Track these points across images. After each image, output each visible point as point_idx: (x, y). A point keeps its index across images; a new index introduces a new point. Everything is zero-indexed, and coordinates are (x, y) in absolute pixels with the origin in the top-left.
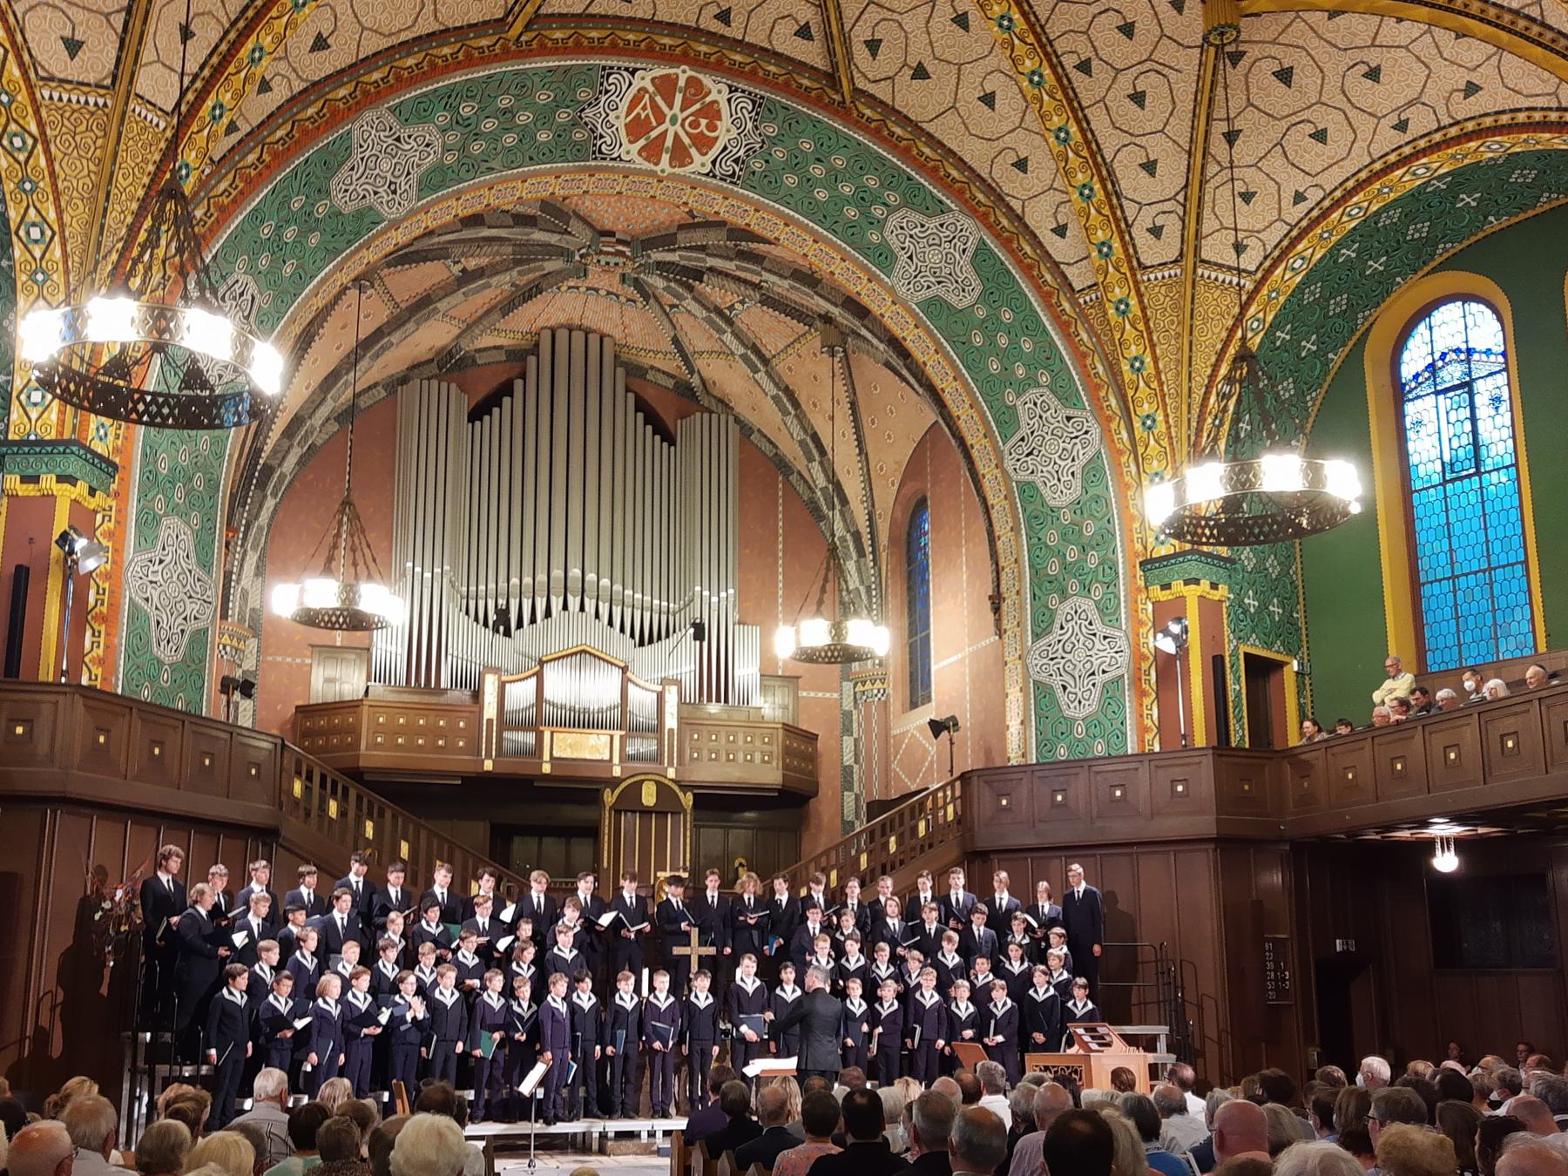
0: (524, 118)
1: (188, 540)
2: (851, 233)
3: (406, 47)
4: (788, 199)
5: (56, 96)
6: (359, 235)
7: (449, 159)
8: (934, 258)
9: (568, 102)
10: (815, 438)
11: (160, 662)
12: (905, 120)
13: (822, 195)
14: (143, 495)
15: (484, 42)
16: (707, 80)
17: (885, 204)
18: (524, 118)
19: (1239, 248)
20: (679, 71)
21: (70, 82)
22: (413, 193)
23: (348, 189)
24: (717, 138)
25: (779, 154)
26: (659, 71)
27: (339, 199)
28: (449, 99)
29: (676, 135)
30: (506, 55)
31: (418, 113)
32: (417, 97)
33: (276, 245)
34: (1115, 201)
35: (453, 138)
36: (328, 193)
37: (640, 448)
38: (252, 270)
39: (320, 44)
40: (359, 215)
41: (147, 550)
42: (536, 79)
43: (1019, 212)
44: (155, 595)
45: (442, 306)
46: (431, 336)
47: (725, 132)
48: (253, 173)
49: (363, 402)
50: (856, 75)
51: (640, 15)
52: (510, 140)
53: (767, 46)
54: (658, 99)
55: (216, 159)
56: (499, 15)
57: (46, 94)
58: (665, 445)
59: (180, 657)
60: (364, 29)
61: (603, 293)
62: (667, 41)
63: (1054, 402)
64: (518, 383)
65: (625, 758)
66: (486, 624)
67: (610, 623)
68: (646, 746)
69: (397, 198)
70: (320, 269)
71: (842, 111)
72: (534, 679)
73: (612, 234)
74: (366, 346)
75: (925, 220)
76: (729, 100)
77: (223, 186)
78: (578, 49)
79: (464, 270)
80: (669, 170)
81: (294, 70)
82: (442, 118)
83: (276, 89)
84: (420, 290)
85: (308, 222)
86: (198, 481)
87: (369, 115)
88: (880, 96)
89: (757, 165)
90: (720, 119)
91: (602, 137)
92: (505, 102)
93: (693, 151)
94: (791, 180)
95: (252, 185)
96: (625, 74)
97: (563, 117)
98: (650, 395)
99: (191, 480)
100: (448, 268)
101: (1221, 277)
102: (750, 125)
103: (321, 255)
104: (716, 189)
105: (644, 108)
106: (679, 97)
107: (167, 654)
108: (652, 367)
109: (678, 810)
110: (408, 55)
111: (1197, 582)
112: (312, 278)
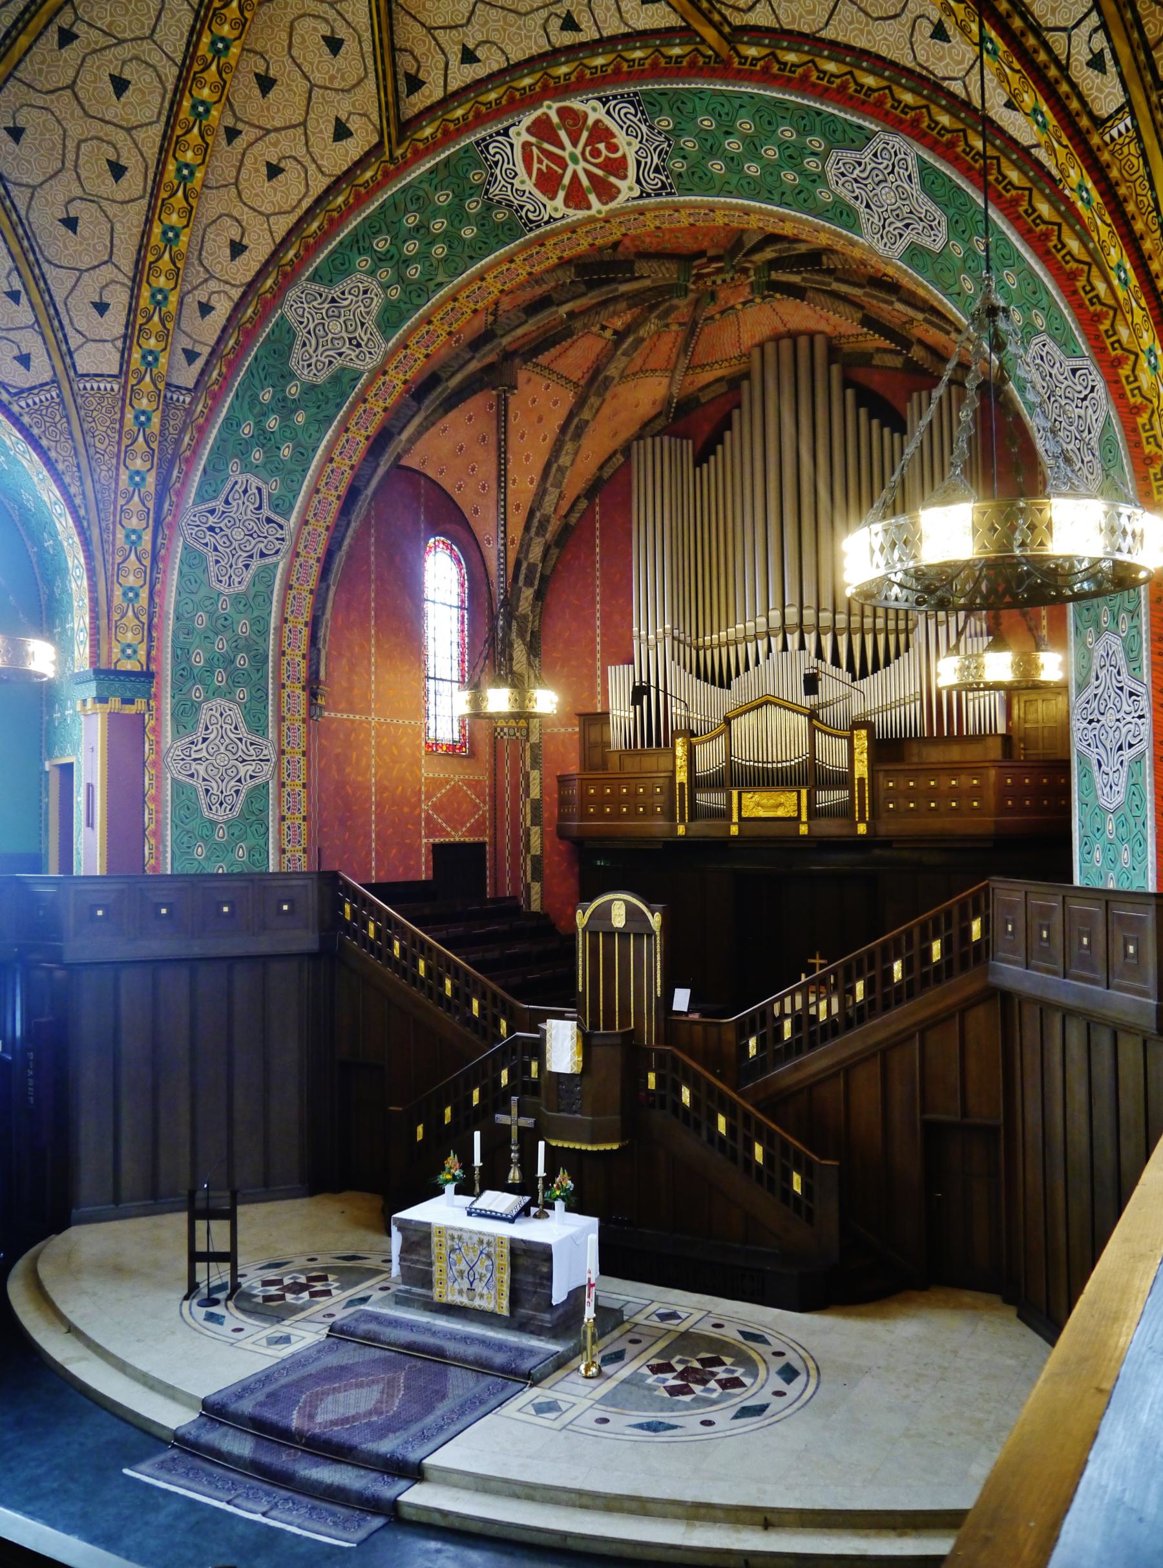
0: (439, 225)
1: (236, 714)
2: (801, 198)
3: (310, 213)
4: (727, 188)
5: (30, 402)
6: (344, 396)
7: (395, 293)
8: (887, 196)
9: (468, 192)
10: (564, 429)
11: (213, 823)
12: (797, 39)
13: (753, 169)
14: (177, 688)
16: (575, 104)
17: (814, 154)
18: (439, 225)
20: (544, 110)
21: (34, 388)
23: (309, 365)
24: (624, 157)
25: (689, 144)
26: (528, 120)
27: (306, 375)
28: (358, 243)
29: (586, 171)
30: (388, 177)
31: (338, 269)
33: (263, 438)
36: (292, 376)
37: (729, 495)
38: (248, 468)
39: (237, 249)
40: (335, 379)
41: (189, 735)
43: (963, 95)
45: (612, 371)
46: (644, 395)
47: (627, 147)
49: (607, 472)
50: (727, 12)
51: (495, 67)
52: (439, 250)
53: (627, 30)
54: (546, 146)
55: (191, 385)
56: (375, 139)
57: (23, 404)
60: (268, 216)
61: (717, 316)
63: (1057, 353)
64: (736, 413)
65: (813, 813)
66: (698, 677)
67: (836, 662)
69: (364, 349)
70: (320, 440)
71: (721, 68)
72: (721, 740)
73: (701, 254)
74: (572, 428)
75: (856, 155)
76: (608, 113)
77: (200, 407)
78: (448, 137)
79: (616, 332)
80: (605, 208)
82: (363, 262)
83: (218, 306)
84: (589, 364)
85: (286, 408)
87: (292, 294)
88: (320, 190)
89: (678, 165)
90: (613, 136)
91: (522, 207)
92: (411, 221)
94: (717, 167)
96: (499, 138)
97: (473, 206)
98: (875, 381)
99: (232, 662)
100: (599, 336)
102: (644, 128)
103: (313, 429)
105: (540, 161)
107: (220, 815)
108: (878, 350)
109: (651, 934)
110: (313, 220)
112: (315, 450)
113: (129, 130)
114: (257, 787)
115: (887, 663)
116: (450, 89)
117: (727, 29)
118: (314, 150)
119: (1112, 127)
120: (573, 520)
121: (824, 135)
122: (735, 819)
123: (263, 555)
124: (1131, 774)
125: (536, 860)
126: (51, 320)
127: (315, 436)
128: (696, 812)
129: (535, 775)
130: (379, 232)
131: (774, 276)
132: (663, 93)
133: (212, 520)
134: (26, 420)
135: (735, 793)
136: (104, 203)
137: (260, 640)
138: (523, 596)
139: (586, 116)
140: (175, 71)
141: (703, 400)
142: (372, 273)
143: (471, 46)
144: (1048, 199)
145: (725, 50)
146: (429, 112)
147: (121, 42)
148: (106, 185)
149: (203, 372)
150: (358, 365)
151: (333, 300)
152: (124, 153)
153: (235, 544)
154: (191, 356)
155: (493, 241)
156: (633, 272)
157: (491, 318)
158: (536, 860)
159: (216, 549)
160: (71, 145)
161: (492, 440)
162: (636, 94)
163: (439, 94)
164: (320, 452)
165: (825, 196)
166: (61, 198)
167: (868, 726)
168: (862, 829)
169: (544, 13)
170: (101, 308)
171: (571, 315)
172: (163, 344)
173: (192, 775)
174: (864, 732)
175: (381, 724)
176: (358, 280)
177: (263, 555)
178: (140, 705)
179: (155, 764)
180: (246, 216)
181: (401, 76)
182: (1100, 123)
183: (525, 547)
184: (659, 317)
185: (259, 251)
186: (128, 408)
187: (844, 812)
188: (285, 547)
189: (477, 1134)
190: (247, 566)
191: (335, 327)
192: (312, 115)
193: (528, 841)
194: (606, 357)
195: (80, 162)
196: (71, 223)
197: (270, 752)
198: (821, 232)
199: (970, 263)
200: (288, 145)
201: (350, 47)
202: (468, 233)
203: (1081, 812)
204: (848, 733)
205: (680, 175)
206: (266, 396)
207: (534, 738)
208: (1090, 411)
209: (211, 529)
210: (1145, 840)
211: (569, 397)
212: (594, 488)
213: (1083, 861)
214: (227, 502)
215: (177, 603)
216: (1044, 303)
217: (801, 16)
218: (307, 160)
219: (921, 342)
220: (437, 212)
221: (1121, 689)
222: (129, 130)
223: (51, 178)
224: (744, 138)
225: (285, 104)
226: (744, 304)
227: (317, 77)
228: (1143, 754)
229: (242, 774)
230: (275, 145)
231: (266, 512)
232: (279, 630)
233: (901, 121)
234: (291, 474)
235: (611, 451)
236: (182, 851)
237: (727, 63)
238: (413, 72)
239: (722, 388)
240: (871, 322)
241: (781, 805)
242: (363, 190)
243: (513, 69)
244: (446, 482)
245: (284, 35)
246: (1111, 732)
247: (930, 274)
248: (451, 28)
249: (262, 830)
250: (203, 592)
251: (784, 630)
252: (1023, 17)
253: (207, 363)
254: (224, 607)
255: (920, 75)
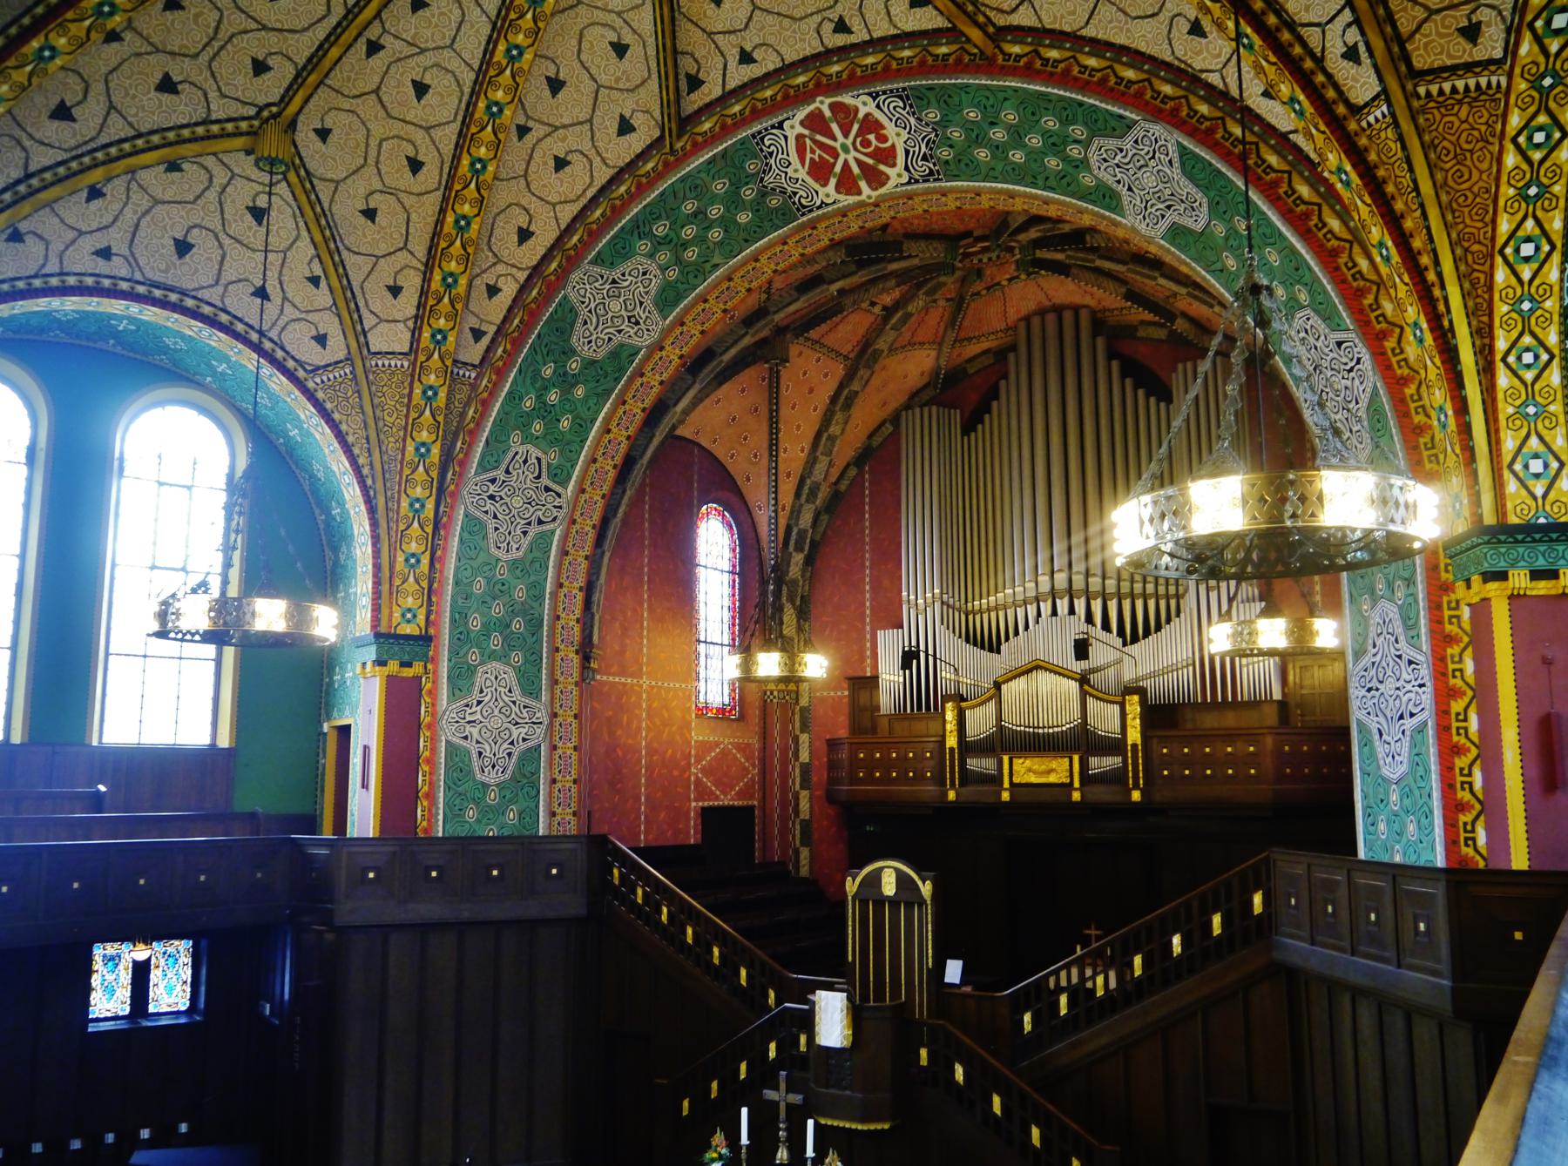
0: (715, 211)
1: (510, 677)
2: (1065, 182)
3: (594, 202)
6: (622, 370)
7: (673, 274)
8: (1149, 180)
10: (834, 399)
11: (485, 786)
13: (1018, 156)
14: (454, 653)
15: (650, 165)
16: (847, 99)
17: (1076, 141)
18: (715, 211)
19: (1471, 32)
22: (656, 315)
23: (589, 343)
24: (893, 146)
25: (956, 134)
26: (802, 114)
27: (586, 352)
28: (639, 228)
29: (857, 160)
30: (668, 167)
31: (619, 252)
32: (609, 243)
33: (545, 411)
34: (1286, 36)
35: (664, 256)
36: (574, 352)
37: (1104, 422)
38: (528, 439)
39: (524, 235)
40: (614, 355)
42: (703, 175)
43: (1221, 86)
44: (475, 732)
45: (881, 345)
46: (914, 366)
47: (896, 137)
48: (500, 363)
50: (991, 14)
51: (771, 67)
52: (716, 234)
54: (819, 137)
56: (657, 133)
57: (318, 380)
58: (1162, 405)
59: (507, 776)
60: (554, 205)
62: (801, 79)
63: (1322, 327)
64: (1003, 383)
65: (1086, 779)
68: (1111, 762)
69: (643, 326)
70: (598, 412)
72: (992, 705)
73: (969, 234)
74: (842, 399)
76: (878, 106)
78: (725, 131)
79: (885, 308)
80: (875, 194)
81: (513, 266)
82: (643, 246)
85: (566, 382)
86: (517, 625)
87: (575, 276)
88: (604, 181)
89: (945, 154)
90: (883, 127)
91: (795, 194)
92: (689, 207)
93: (882, 167)
94: (983, 154)
95: (501, 373)
97: (748, 193)
99: (508, 626)
101: (1460, 84)
102: (912, 120)
104: (927, 192)
105: (813, 152)
106: (835, 127)
107: (491, 777)
108: (1143, 322)
109: (922, 902)
111: (1502, 576)
112: (593, 421)
113: (427, 129)
114: (529, 750)
115: (1158, 628)
116: (729, 87)
117: (991, 30)
118: (599, 144)
119: (1368, 114)
120: (843, 487)
121: (1086, 124)
122: (1006, 784)
123: (540, 522)
124: (1413, 744)
125: (806, 825)
126: (348, 303)
127: (594, 408)
128: (967, 777)
129: (804, 738)
130: (659, 218)
131: (1039, 254)
132: (930, 88)
133: (492, 489)
134: (320, 395)
135: (1006, 759)
136: (401, 195)
137: (535, 605)
138: (793, 561)
139: (857, 110)
140: (472, 76)
141: (971, 371)
142: (651, 256)
143: (748, 48)
144: (1306, 180)
145: (989, 49)
146: (708, 108)
147: (423, 51)
148: (405, 179)
149: (488, 350)
150: (636, 341)
151: (614, 281)
152: (422, 150)
153: (514, 512)
154: (477, 334)
155: (767, 224)
156: (901, 251)
157: (764, 296)
158: (806, 825)
159: (495, 517)
160: (373, 143)
161: (764, 411)
162: (904, 89)
163: (717, 92)
164: (598, 424)
165: (1087, 180)
166: (362, 192)
167: (1141, 692)
168: (1136, 796)
169: (818, 18)
170: (395, 291)
171: (841, 292)
172: (451, 324)
173: (466, 738)
174: (1136, 698)
175: (652, 687)
176: (639, 262)
177: (540, 522)
178: (417, 669)
179: (429, 727)
180: (535, 205)
181: (682, 76)
182: (1356, 110)
183: (796, 513)
184: (926, 294)
185: (544, 237)
186: (417, 384)
187: (1116, 778)
188: (561, 514)
189: (744, 1111)
190: (525, 533)
191: (615, 306)
192: (598, 113)
193: (797, 805)
194: (877, 330)
195: (382, 158)
196: (370, 214)
197: (543, 715)
198: (1087, 214)
199: (1231, 242)
200: (576, 139)
201: (635, 51)
202: (743, 218)
203: (1363, 780)
204: (1119, 699)
205: (947, 162)
206: (548, 371)
207: (804, 702)
208: (1357, 382)
209: (492, 497)
210: (1431, 812)
211: (840, 370)
212: (864, 456)
213: (1367, 832)
214: (507, 472)
215: (457, 569)
216: (1307, 279)
217: (1062, 17)
218: (592, 153)
219: (1184, 315)
220: (714, 199)
221: (1400, 657)
222: (427, 129)
223: (354, 173)
224: (1010, 128)
225: (572, 103)
226: (1010, 280)
227: (603, 79)
228: (1425, 723)
229: (515, 736)
230: (563, 140)
231: (545, 481)
232: (554, 595)
233: (1161, 111)
234: (568, 445)
235: (880, 420)
236: (453, 814)
237: (991, 61)
238: (693, 72)
239: (989, 360)
240: (1134, 296)
241: (1052, 770)
242: (644, 180)
243: (788, 69)
244: (720, 452)
245: (574, 42)
246: (1391, 701)
247: (1193, 251)
248: (730, 32)
249: (534, 793)
250: (482, 557)
251: (1053, 594)
252: (1279, 16)
253: (493, 341)
254: (502, 572)
255: (1178, 69)
